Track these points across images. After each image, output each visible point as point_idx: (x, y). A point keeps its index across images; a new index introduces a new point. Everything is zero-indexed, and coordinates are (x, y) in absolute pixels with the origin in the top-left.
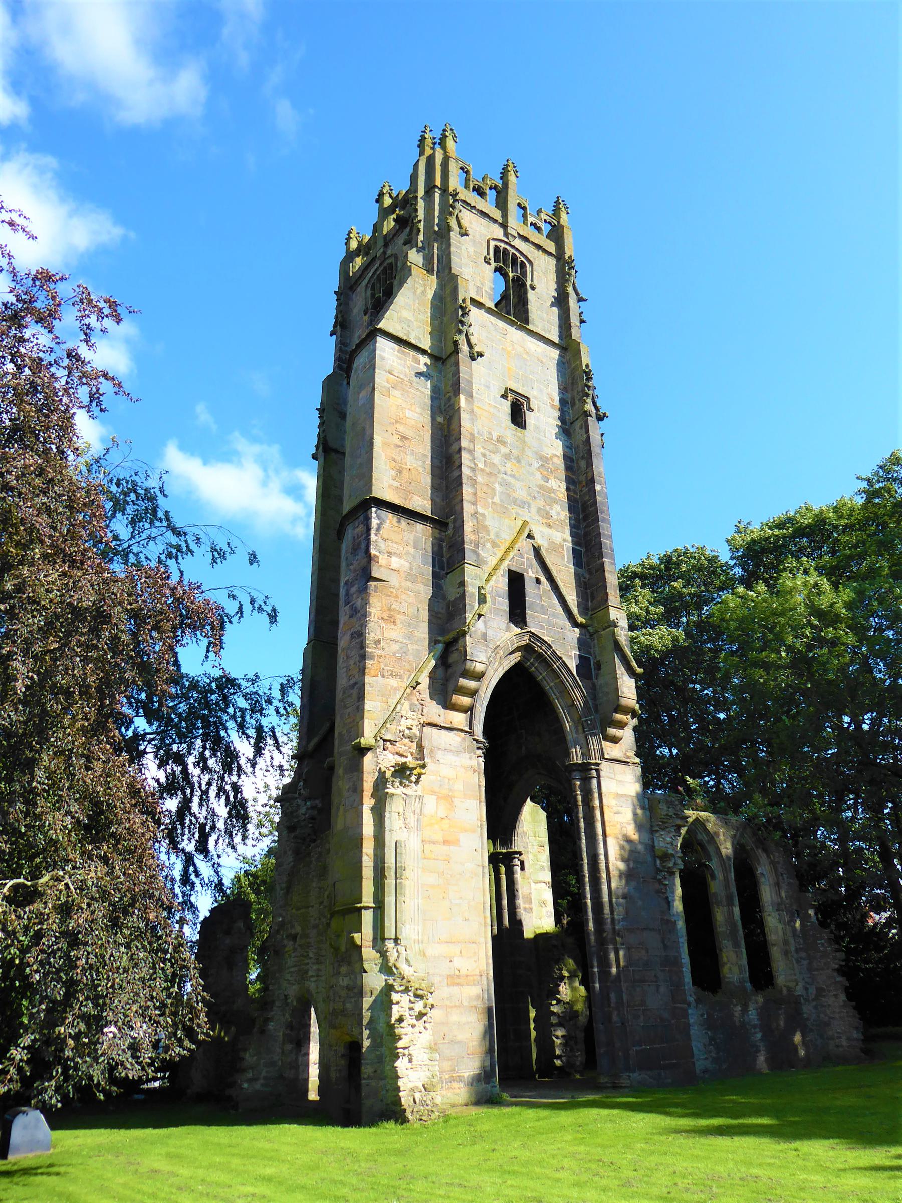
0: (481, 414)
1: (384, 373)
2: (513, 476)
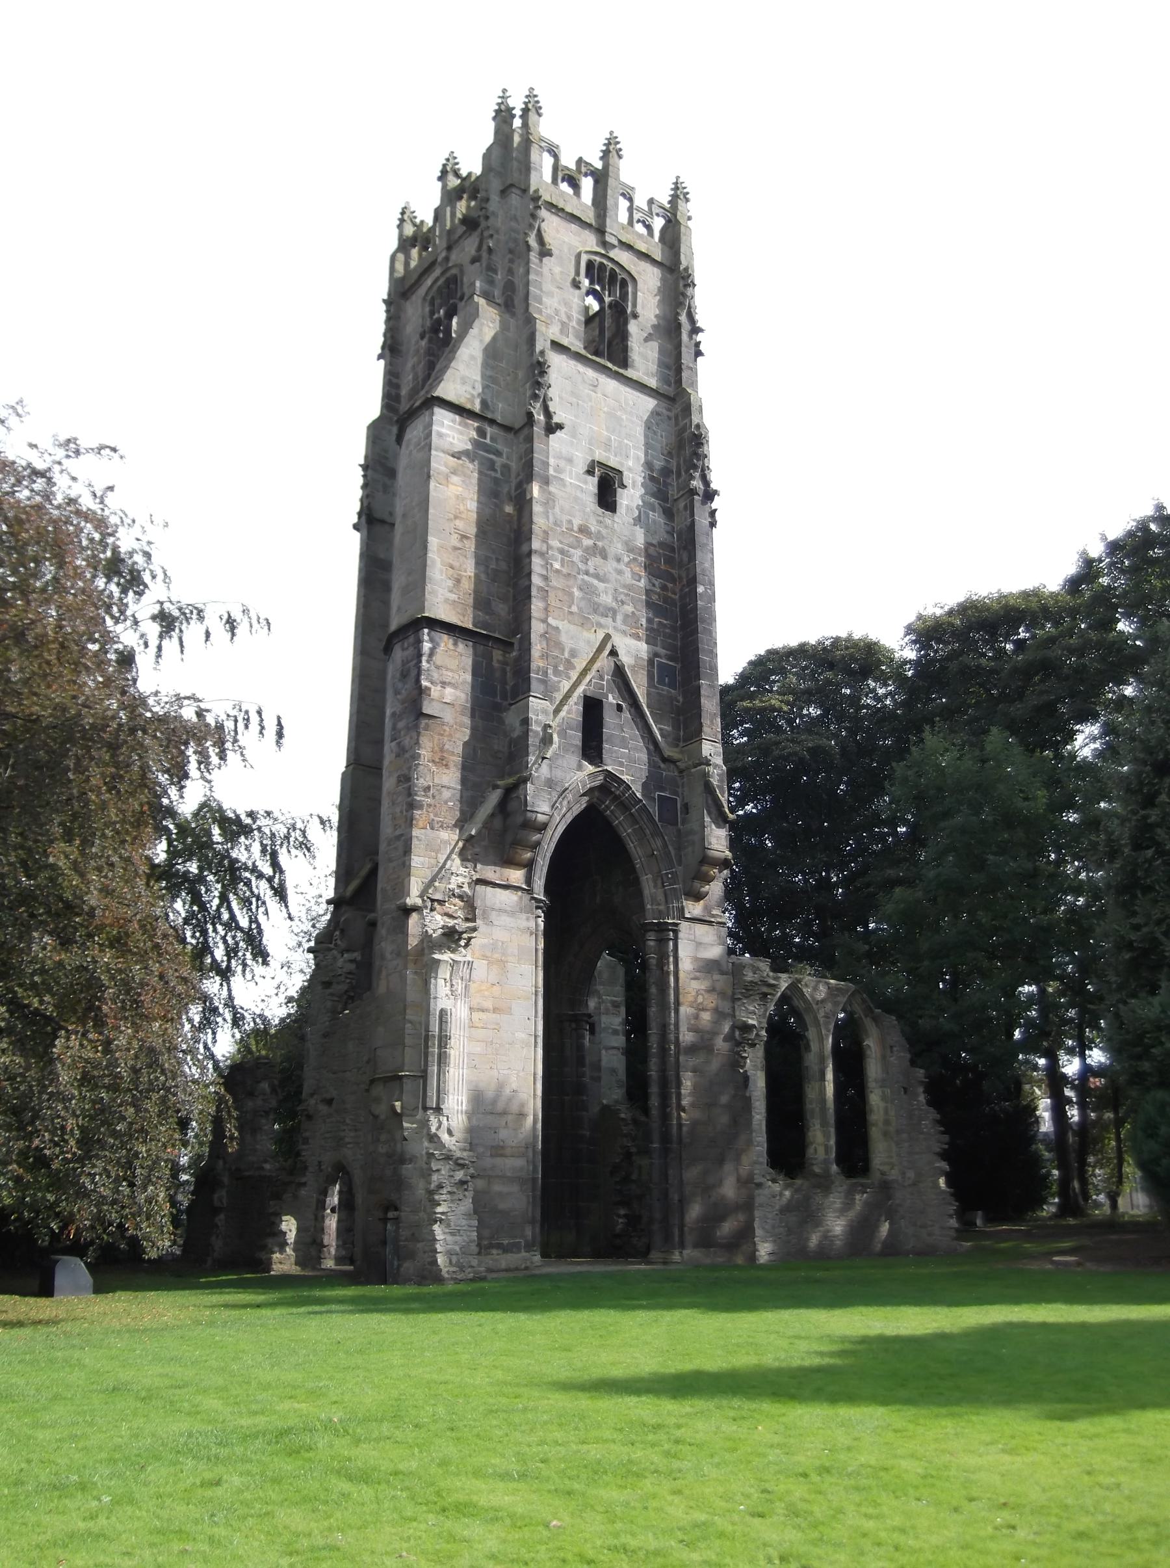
0: (561, 497)
1: (442, 455)
2: (597, 576)
